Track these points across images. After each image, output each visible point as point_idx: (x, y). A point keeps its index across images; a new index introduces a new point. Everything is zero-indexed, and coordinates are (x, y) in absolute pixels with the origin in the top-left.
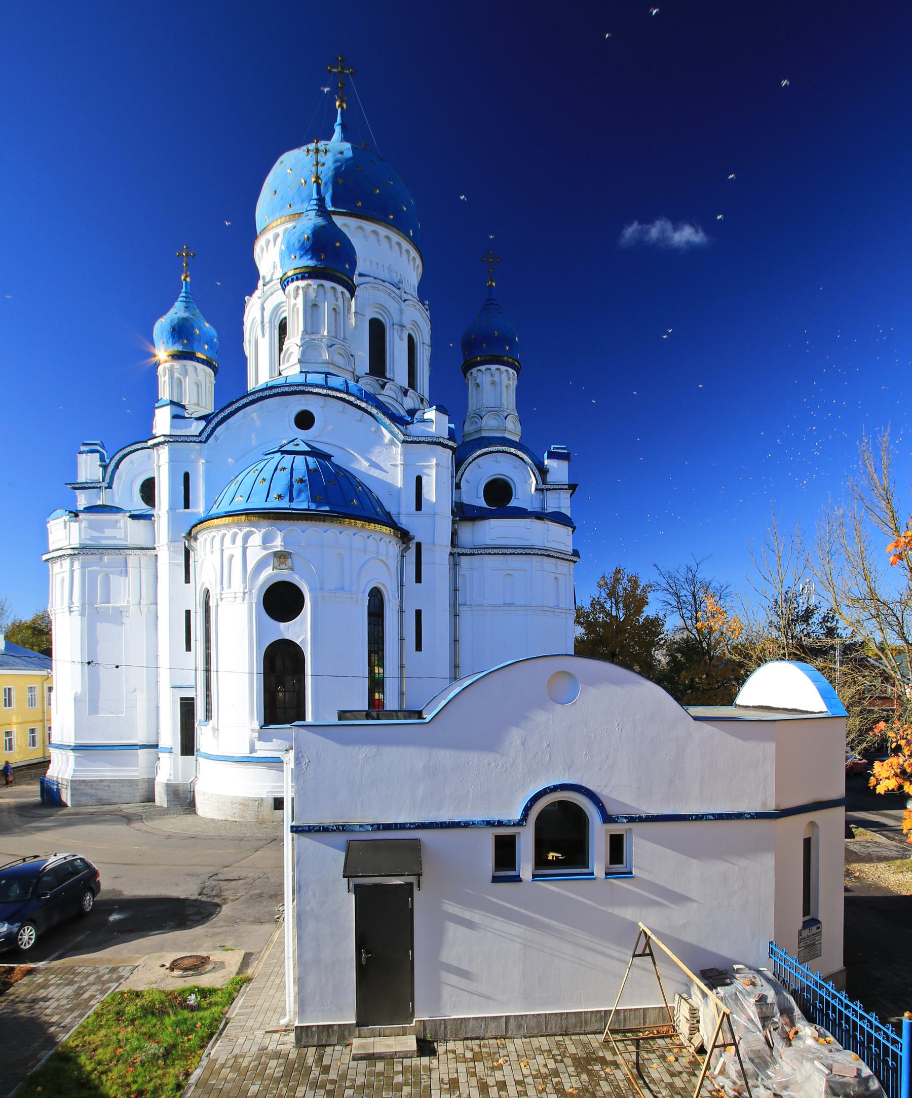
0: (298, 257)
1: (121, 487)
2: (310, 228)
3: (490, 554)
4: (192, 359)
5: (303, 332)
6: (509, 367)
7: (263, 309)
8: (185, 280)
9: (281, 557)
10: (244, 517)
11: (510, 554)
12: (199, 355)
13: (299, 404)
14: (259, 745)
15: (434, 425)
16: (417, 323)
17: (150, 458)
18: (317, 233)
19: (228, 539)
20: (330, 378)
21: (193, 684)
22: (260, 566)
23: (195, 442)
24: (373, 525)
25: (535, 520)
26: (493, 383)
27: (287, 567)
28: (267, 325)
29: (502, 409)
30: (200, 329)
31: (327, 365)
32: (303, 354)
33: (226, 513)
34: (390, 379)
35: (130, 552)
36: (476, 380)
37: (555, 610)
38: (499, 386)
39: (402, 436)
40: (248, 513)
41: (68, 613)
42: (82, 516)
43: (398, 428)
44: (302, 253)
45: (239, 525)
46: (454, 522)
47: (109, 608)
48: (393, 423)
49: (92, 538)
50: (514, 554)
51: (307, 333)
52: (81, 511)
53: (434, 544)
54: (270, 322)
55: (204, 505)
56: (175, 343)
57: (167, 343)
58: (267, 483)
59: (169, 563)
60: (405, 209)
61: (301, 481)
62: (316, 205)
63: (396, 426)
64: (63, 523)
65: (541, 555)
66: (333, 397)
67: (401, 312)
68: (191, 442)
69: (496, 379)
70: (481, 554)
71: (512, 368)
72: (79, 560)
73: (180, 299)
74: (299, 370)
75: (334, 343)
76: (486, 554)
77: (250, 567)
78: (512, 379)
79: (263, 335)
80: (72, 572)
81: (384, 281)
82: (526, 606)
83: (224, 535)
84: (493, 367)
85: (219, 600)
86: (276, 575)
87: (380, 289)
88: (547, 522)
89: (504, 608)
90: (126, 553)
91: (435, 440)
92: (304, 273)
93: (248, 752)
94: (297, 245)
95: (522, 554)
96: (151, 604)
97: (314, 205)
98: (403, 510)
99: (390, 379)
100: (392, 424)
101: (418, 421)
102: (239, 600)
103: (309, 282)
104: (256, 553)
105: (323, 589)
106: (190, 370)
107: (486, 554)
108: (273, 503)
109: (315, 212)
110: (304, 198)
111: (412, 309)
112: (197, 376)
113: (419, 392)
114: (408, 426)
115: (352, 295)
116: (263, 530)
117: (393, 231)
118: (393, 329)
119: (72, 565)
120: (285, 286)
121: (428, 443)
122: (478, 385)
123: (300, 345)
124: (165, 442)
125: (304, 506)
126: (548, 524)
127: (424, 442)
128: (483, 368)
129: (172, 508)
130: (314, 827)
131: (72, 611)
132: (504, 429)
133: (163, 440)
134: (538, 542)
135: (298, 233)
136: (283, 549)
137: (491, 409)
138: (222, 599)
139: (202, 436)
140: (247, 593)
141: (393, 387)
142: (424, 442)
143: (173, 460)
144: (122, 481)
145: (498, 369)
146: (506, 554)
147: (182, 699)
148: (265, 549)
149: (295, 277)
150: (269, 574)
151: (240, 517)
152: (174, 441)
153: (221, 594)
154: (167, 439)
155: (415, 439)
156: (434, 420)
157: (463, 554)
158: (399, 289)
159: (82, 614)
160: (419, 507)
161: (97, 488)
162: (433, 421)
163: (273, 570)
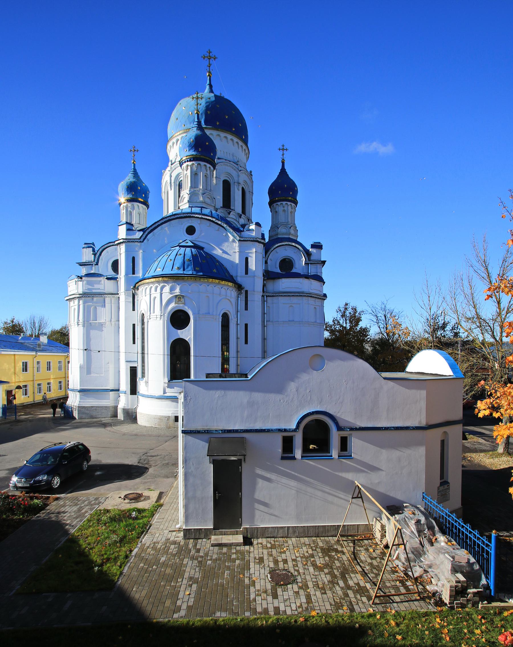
0: (188, 150)
3: (282, 296)
7: (171, 176)
8: (133, 163)
9: (178, 298)
11: (292, 296)
14: (168, 390)
19: (153, 289)
23: (137, 242)
24: (224, 281)
26: (284, 211)
28: (173, 184)
29: (288, 224)
32: (190, 198)
33: (152, 276)
34: (233, 210)
35: (106, 296)
38: (287, 212)
41: (77, 325)
43: (237, 234)
44: (190, 148)
45: (158, 282)
46: (264, 280)
49: (89, 289)
52: (83, 276)
53: (254, 291)
54: (174, 183)
57: (125, 194)
60: (240, 125)
62: (197, 124)
63: (235, 233)
64: (75, 282)
65: (308, 296)
66: (205, 219)
69: (285, 208)
70: (278, 296)
72: (82, 300)
75: (205, 192)
79: (171, 189)
80: (79, 306)
81: (230, 161)
82: (300, 322)
83: (152, 287)
84: (284, 203)
85: (149, 319)
86: (176, 307)
88: (311, 280)
91: (255, 239)
95: (298, 296)
98: (239, 274)
99: (233, 210)
102: (158, 319)
103: (193, 162)
105: (199, 313)
106: (136, 207)
108: (175, 271)
109: (196, 128)
119: (79, 302)
121: (252, 241)
122: (276, 212)
124: (123, 242)
125: (190, 272)
127: (249, 241)
128: (279, 203)
129: (127, 274)
136: (180, 294)
138: (150, 319)
141: (234, 214)
142: (249, 241)
143: (127, 251)
146: (290, 296)
147: (131, 367)
148: (171, 294)
152: (128, 242)
154: (124, 241)
156: (254, 229)
158: (237, 165)
159: (84, 326)
160: (247, 273)
161: (91, 265)
163: (175, 304)
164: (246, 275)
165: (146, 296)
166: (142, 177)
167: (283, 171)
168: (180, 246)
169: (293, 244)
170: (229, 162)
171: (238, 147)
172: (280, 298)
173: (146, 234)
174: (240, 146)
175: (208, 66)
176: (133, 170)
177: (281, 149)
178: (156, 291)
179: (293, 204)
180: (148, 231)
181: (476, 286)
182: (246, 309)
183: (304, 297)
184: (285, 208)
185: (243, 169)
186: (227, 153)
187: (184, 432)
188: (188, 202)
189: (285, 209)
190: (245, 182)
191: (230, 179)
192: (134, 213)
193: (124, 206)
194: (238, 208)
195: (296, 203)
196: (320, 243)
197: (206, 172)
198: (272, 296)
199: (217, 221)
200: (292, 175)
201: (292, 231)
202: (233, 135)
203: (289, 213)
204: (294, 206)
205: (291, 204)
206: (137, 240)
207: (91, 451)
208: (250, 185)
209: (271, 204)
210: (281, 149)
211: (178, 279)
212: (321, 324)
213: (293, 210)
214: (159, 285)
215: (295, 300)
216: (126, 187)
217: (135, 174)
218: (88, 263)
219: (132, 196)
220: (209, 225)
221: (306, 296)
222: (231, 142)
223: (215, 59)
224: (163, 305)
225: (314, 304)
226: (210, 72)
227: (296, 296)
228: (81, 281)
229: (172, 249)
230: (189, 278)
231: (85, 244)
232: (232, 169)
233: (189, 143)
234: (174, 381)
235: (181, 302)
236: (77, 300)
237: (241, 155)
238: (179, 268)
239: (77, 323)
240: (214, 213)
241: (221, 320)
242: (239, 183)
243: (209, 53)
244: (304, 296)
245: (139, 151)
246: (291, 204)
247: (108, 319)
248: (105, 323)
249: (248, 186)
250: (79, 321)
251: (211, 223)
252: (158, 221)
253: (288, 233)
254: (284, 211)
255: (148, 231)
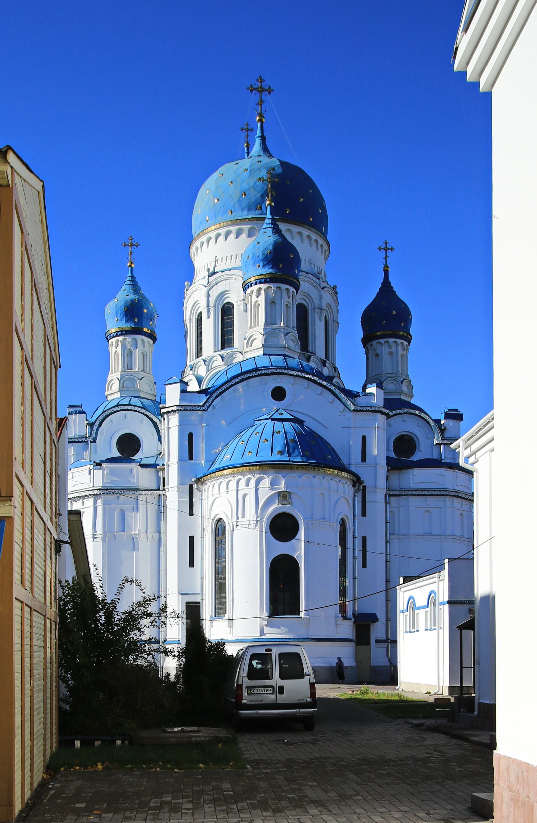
0: (261, 266)
1: (102, 442)
2: (271, 244)
3: (414, 495)
4: (141, 334)
5: (265, 323)
6: (404, 340)
7: (209, 296)
8: (130, 266)
9: (284, 496)
10: (258, 467)
11: (430, 495)
12: (145, 330)
13: (274, 382)
14: (266, 630)
15: (375, 398)
16: (308, 295)
17: (126, 418)
18: (276, 246)
19: (243, 483)
20: (289, 360)
21: (200, 592)
22: (269, 502)
23: (199, 410)
24: (343, 473)
25: (448, 469)
26: (391, 353)
27: (288, 503)
28: (212, 309)
29: (398, 375)
30: (147, 309)
31: (284, 349)
32: (266, 341)
33: (243, 464)
34: (311, 353)
35: (142, 492)
36: (375, 351)
37: (462, 539)
38: (395, 356)
39: (353, 406)
40: (244, 465)
41: (92, 539)
42: (104, 465)
43: (350, 401)
44: (265, 263)
45: (242, 473)
46: (388, 470)
47: (124, 535)
48: (347, 397)
49: (112, 482)
50: (432, 495)
51: (267, 325)
52: (104, 462)
53: (375, 487)
54: (215, 306)
55: (205, 457)
56: (128, 321)
57: (121, 320)
58: (269, 442)
59: (178, 501)
60: (320, 211)
61: (294, 441)
62: (271, 223)
63: (349, 399)
64: (88, 470)
65: (453, 496)
66: (302, 377)
67: (321, 297)
68: (197, 410)
69: (393, 350)
70: (407, 495)
71: (406, 341)
72: (101, 498)
73: (126, 283)
74: (262, 353)
75: (288, 331)
76: (411, 495)
77: (261, 504)
78: (291, 298)
79: (209, 317)
80: (95, 508)
81: (308, 273)
82: (440, 535)
83: (240, 479)
84: (391, 340)
85: (235, 526)
86: (280, 508)
87: (305, 280)
88: (456, 471)
89: (425, 537)
90: (126, 492)
91: (377, 409)
92: (266, 278)
93: (259, 635)
94: (261, 257)
95: (438, 495)
96: (154, 532)
97: (269, 223)
98: (353, 461)
99: (311, 353)
100: (345, 397)
101: (364, 395)
102: (252, 526)
103: (271, 285)
104: (266, 491)
105: (312, 519)
106: (140, 343)
107: (411, 495)
108: (277, 457)
109: (271, 229)
110: (244, 207)
111: (327, 294)
112: (144, 347)
113: (330, 361)
114: (356, 398)
115: (297, 290)
116: (271, 477)
117: (304, 228)
118: (315, 311)
119: (95, 502)
120: (248, 287)
121: (372, 411)
122: (377, 355)
123: (263, 334)
124: (178, 410)
125: (299, 459)
126: (457, 472)
127: (369, 411)
128: (382, 341)
129: (180, 460)
130: (457, 601)
131: (96, 538)
132: (401, 392)
133: (176, 409)
134: (449, 486)
135: (262, 249)
136: (285, 490)
137: (390, 375)
138: (237, 526)
139: (205, 406)
140: (259, 521)
141: (315, 360)
142: (369, 411)
143: (182, 424)
144: (103, 436)
145: (395, 342)
146: (426, 495)
147: (187, 603)
148: (272, 489)
149: (258, 281)
150: (274, 508)
151: (255, 467)
152: (184, 410)
153: (237, 522)
154: (179, 408)
155: (363, 408)
156: (375, 394)
157: (393, 495)
158: (319, 279)
159: (104, 540)
160: (364, 459)
161: (84, 442)
162: (374, 395)
163: (278, 505)
164: (363, 463)
165: (228, 492)
166: (145, 290)
167: (386, 286)
168: (273, 419)
169: (417, 412)
170: (306, 275)
172: (411, 498)
173: (212, 399)
174: (313, 240)
175: (258, 104)
176: (128, 279)
177: (382, 249)
178: (247, 484)
179: (292, 289)
180: (216, 394)
182: (364, 514)
184: (393, 350)
186: (305, 260)
187: (449, 602)
188: (263, 347)
189: (393, 351)
191: (308, 305)
192: (137, 354)
193: (118, 341)
194: (320, 352)
195: (408, 339)
196: (457, 410)
197: (288, 300)
198: (399, 495)
199: (321, 381)
200: (401, 293)
201: (405, 389)
204: (293, 292)
205: (402, 343)
206: (199, 408)
207: (433, 590)
208: (335, 310)
209: (366, 341)
210: (382, 249)
211: (285, 468)
212: (470, 539)
213: (405, 352)
215: (432, 501)
216: (123, 309)
217: (135, 286)
218: (79, 440)
219: (134, 325)
220: (306, 386)
221: (450, 495)
223: (269, 92)
224: (260, 505)
225: (460, 508)
226: (261, 116)
227: (435, 495)
228: (100, 469)
229: (256, 423)
230: (300, 466)
231: (70, 406)
232: (310, 286)
233: (263, 254)
234: (276, 616)
235: (287, 501)
236: (93, 499)
238: (281, 453)
239: (92, 536)
240: (305, 365)
241: (339, 530)
242: (323, 309)
243: (261, 82)
244: (447, 495)
245: (139, 245)
246: (402, 343)
247: (143, 530)
248: (139, 534)
249: (332, 311)
250: (95, 531)
251: (311, 383)
253: (399, 391)
254: (391, 353)
255: (216, 394)
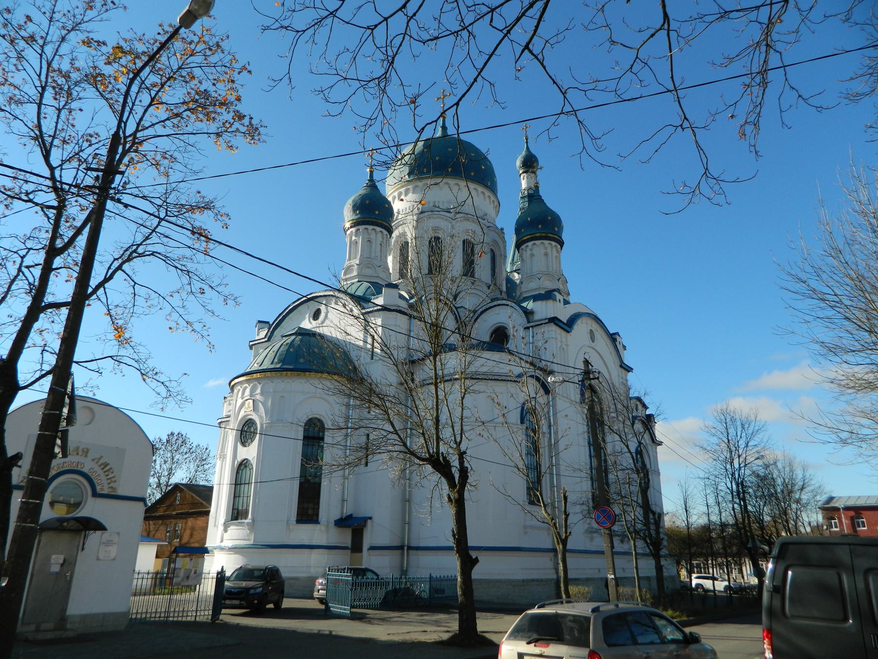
45: (247, 381)
83: (246, 388)
167: (372, 185)
171: (485, 198)
174: (479, 192)
179: (385, 232)
181: (649, 35)
183: (509, 383)
185: (491, 225)
190: (495, 241)
202: (456, 179)
203: (554, 258)
214: (249, 385)
222: (488, 200)
237: (490, 210)
252: (289, 306)
